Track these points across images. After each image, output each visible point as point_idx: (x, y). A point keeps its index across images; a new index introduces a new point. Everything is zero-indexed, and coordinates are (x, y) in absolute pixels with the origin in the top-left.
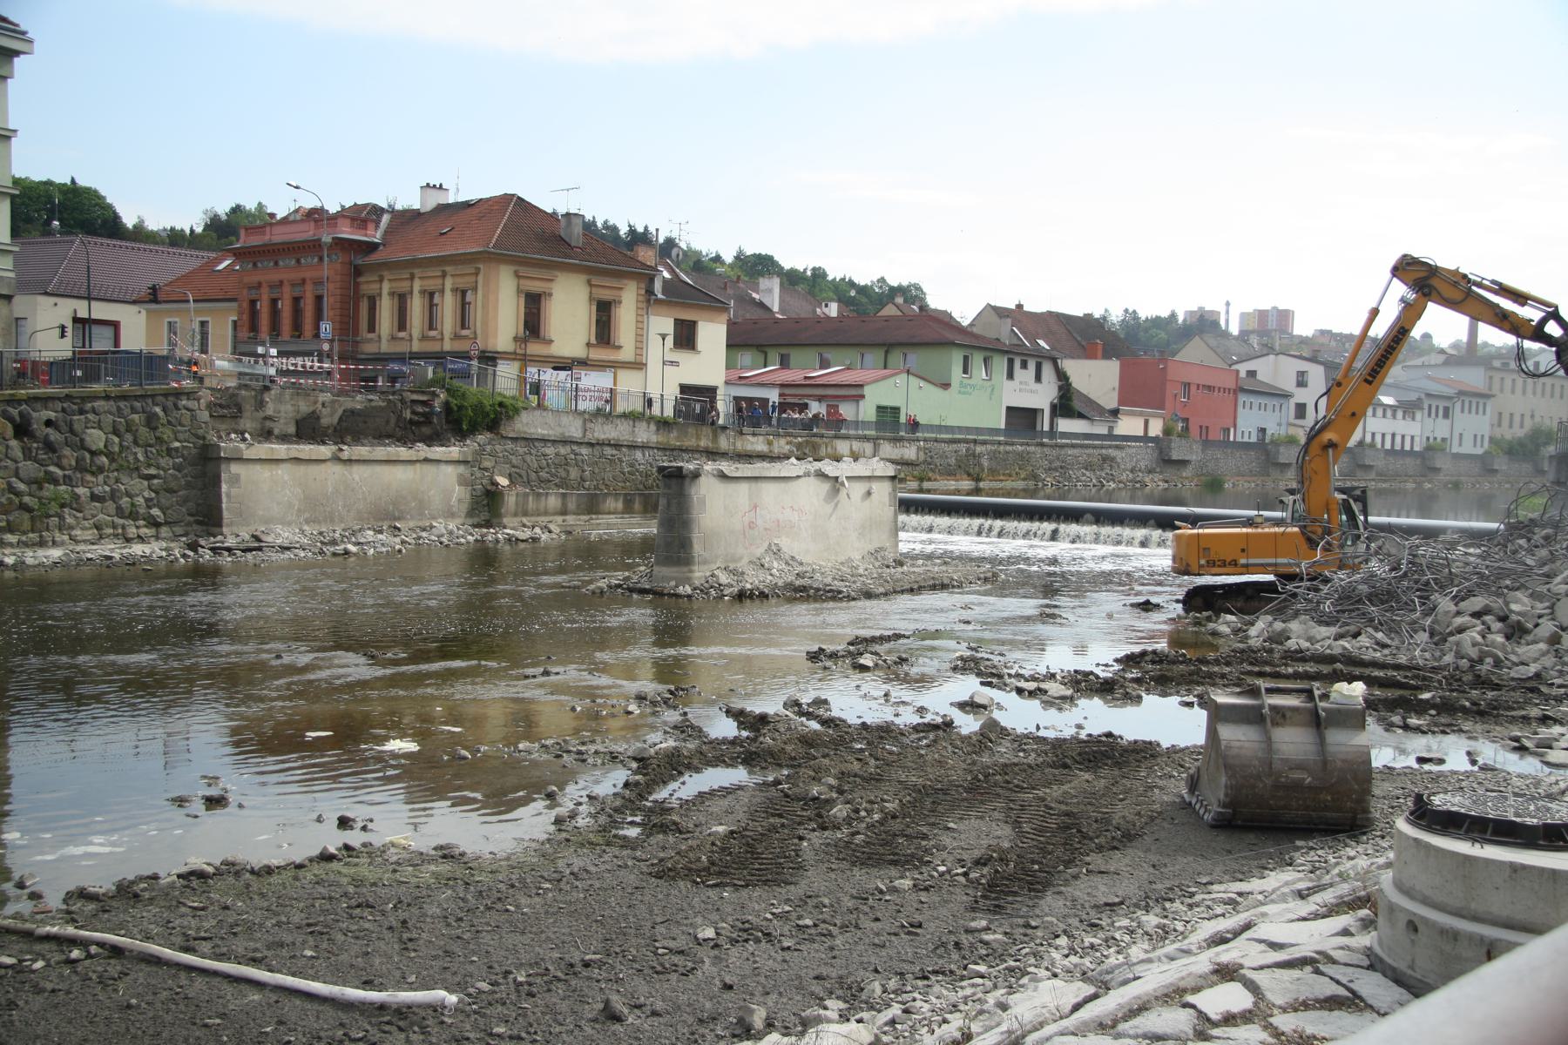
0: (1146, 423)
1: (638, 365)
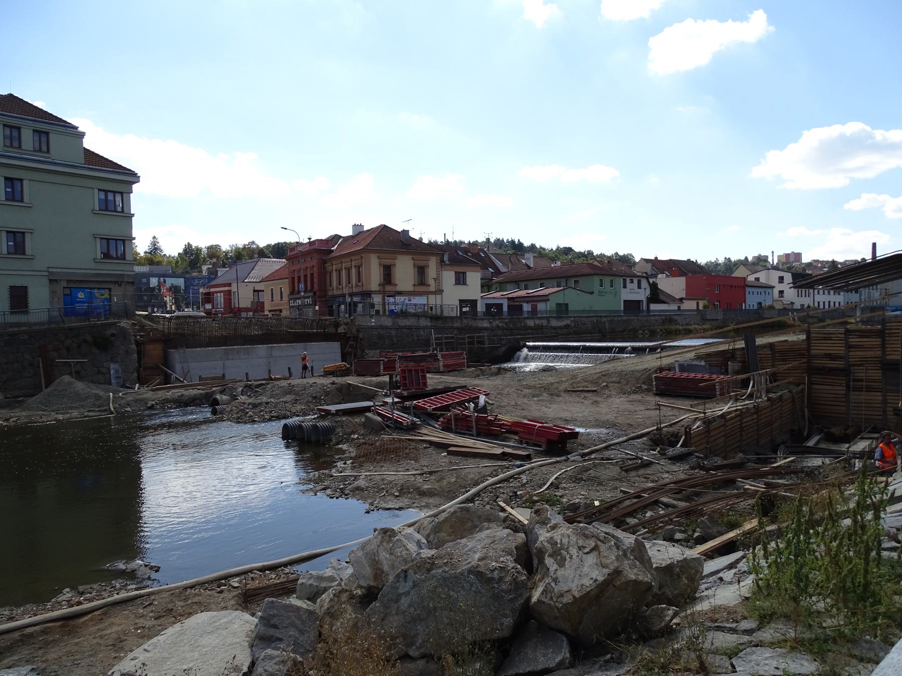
0: (698, 303)
1: (439, 292)
